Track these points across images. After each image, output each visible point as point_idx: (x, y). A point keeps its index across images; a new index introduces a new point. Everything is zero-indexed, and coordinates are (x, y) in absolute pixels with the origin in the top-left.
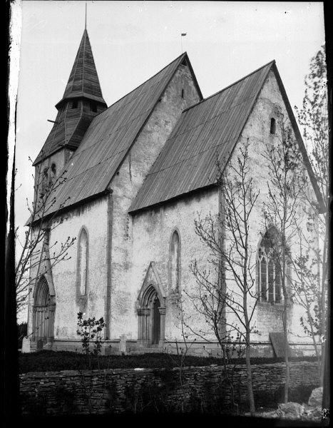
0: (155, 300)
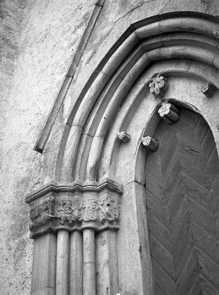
0: (158, 124)
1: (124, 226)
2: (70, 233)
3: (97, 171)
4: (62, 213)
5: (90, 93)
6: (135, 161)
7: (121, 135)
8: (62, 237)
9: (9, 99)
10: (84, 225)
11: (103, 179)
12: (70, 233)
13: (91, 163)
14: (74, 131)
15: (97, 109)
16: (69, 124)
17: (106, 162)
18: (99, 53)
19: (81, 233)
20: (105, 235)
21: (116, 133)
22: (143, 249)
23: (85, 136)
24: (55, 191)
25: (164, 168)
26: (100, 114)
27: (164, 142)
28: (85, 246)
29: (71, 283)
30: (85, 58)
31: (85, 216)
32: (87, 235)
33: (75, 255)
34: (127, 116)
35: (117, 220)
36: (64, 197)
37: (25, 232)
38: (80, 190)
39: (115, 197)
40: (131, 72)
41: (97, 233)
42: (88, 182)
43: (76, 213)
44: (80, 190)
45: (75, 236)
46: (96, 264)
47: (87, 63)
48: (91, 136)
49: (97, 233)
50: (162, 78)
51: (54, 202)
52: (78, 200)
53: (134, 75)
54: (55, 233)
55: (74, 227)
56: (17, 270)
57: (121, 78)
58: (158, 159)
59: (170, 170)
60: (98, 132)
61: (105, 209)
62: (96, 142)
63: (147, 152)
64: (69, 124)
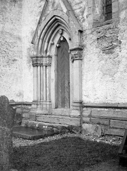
0: (60, 42)
1: (52, 65)
2: (41, 66)
3: (46, 51)
4: (39, 62)
5: (44, 31)
6: (55, 50)
7: (52, 43)
8: (39, 67)
9: (22, 18)
10: (43, 65)
11: (48, 54)
12: (41, 66)
13: (45, 49)
14: (41, 41)
15: (46, 35)
16: (40, 38)
17: (49, 49)
18: (46, 19)
19: (43, 66)
20: (48, 67)
21: (51, 42)
22: (55, 71)
23: (44, 42)
24: (37, 57)
25: (61, 52)
26: (47, 36)
27: (61, 45)
28: (44, 69)
29: (78, 82)
30: (43, 18)
31: (44, 63)
32: (44, 67)
33: (42, 71)
34: (54, 37)
35: (51, 64)
36: (39, 59)
37: (31, 62)
38: (42, 57)
39: (50, 58)
40: (48, 38)
41: (46, 66)
42: (44, 55)
43: (42, 62)
44: (42, 57)
45: (42, 67)
46: (46, 73)
47: (44, 20)
48: (45, 42)
49: (46, 66)
50: (61, 30)
51: (37, 59)
52: (42, 59)
53: (48, 40)
54: (38, 66)
55: (41, 65)
56: (29, 71)
57: (52, 27)
58: (60, 49)
59: (62, 53)
60: (47, 41)
61: (48, 62)
62: (46, 44)
63: (58, 48)
64: (40, 38)
